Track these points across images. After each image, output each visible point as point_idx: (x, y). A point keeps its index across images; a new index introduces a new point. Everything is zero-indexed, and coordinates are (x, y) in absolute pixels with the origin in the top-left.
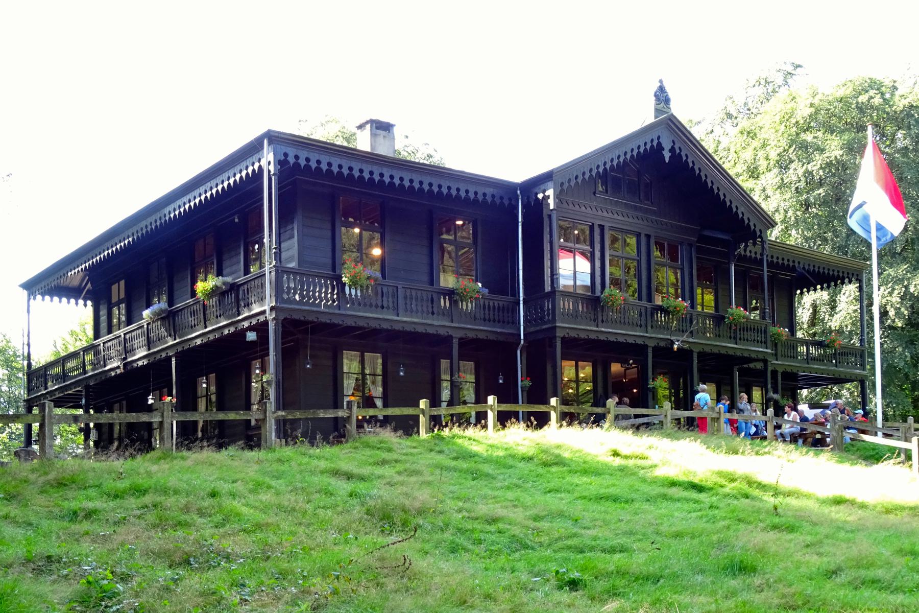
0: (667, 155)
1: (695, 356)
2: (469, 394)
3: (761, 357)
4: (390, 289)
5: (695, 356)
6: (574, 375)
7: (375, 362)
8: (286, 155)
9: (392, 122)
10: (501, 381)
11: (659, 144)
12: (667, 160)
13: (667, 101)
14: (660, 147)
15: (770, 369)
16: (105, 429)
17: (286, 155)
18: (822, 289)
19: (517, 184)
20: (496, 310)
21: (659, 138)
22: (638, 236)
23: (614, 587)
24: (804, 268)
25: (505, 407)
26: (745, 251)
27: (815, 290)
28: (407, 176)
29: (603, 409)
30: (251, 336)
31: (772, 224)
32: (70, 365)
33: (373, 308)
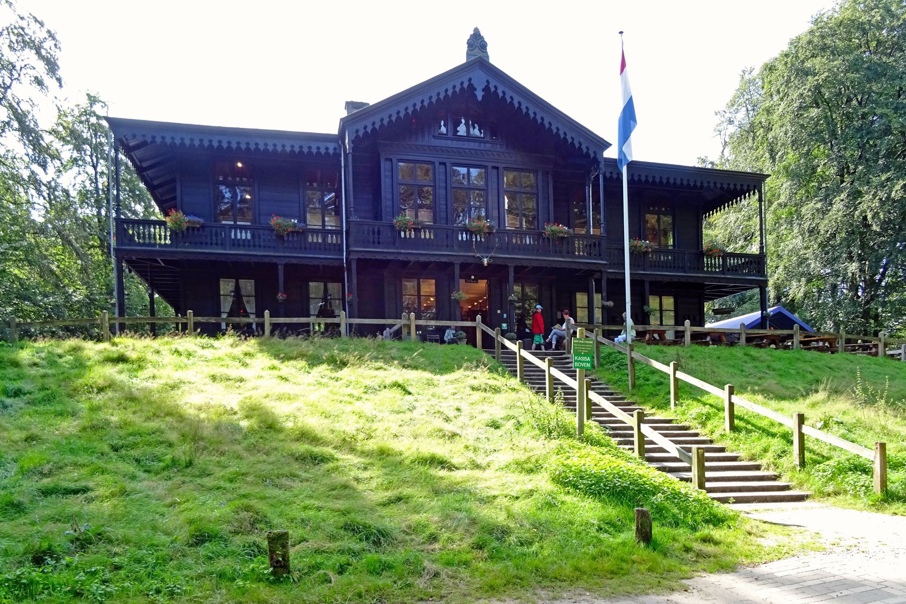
0: (480, 95)
2: (251, 308)
9: (344, 104)
13: (483, 46)
14: (472, 88)
20: (163, 237)
21: (470, 80)
24: (722, 188)
25: (641, 328)
29: (600, 321)
31: (606, 145)
33: (252, 248)
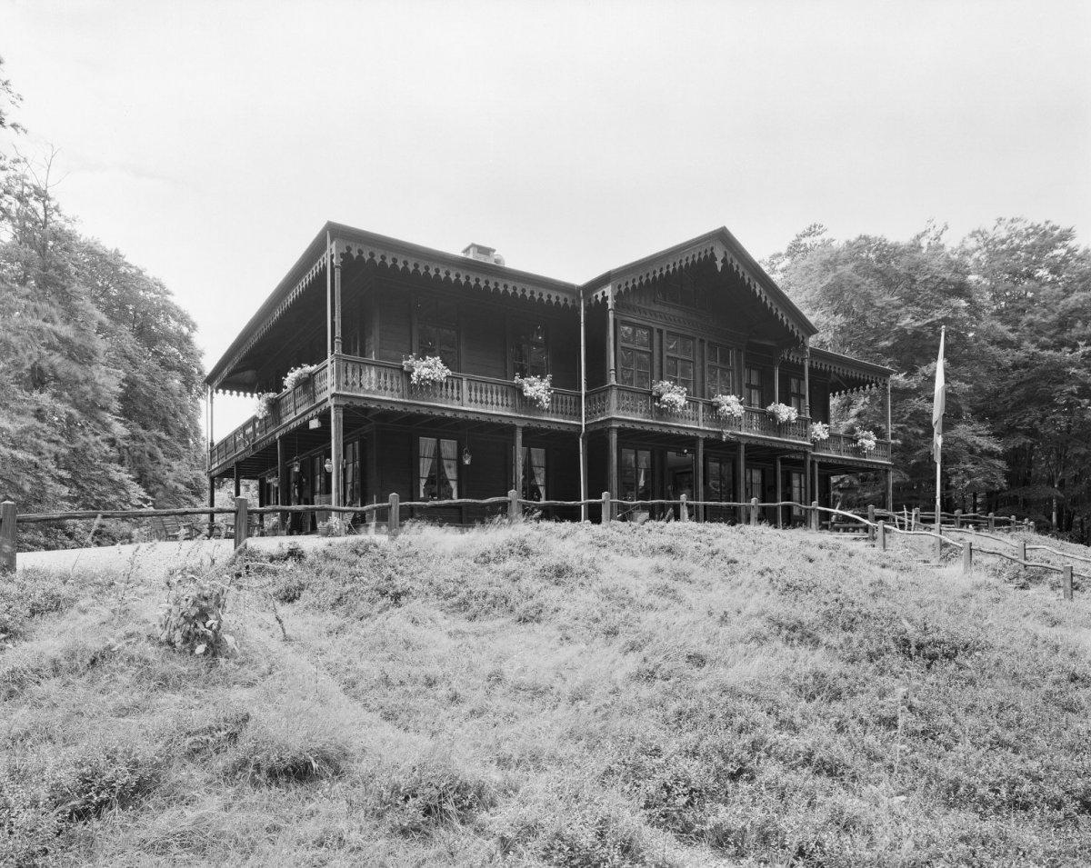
0: (719, 265)
1: (743, 448)
3: (801, 449)
4: (573, 399)
5: (743, 448)
6: (215, 494)
7: (449, 447)
8: (349, 249)
10: (467, 462)
11: (712, 254)
12: (720, 269)
14: (713, 258)
15: (809, 458)
17: (349, 249)
18: (840, 394)
21: (712, 249)
23: (915, 439)
26: (788, 356)
30: (314, 424)
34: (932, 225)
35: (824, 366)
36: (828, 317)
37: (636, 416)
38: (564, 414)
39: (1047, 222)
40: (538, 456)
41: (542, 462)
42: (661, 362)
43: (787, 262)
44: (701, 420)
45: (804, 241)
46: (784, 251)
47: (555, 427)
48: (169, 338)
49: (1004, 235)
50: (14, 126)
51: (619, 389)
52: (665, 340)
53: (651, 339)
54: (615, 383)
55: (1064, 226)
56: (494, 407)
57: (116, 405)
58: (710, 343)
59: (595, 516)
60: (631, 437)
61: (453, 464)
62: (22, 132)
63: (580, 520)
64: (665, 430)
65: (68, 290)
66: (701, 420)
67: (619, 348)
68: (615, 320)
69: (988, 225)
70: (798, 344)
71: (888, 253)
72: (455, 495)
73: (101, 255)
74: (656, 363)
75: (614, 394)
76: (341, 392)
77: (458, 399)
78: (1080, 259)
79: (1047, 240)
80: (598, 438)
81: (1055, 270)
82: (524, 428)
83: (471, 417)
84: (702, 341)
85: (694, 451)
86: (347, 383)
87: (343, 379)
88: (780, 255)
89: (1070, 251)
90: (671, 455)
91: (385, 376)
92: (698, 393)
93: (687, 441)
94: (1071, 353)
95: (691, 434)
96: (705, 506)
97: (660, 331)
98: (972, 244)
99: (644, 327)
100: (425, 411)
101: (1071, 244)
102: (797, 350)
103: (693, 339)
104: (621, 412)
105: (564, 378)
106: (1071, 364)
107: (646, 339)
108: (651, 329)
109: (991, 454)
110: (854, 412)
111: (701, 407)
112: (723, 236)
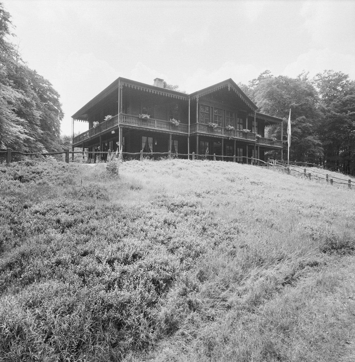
0: (229, 89)
5: (235, 142)
7: (150, 140)
10: (156, 144)
16: (105, 155)
17: (125, 84)
18: (270, 126)
19: (189, 95)
22: (209, 107)
27: (268, 126)
28: (169, 94)
30: (113, 132)
32: (81, 137)
34: (304, 72)
35: (259, 117)
36: (269, 101)
37: (204, 132)
38: (184, 131)
39: (340, 72)
40: (176, 143)
41: (152, 148)
42: (212, 116)
43: (258, 82)
44: (223, 133)
45: (263, 75)
46: (257, 79)
47: (181, 135)
48: (50, 99)
49: (327, 76)
50: (13, 34)
51: (199, 124)
52: (213, 109)
53: (209, 110)
54: (198, 123)
55: (346, 74)
56: (165, 129)
57: (39, 123)
58: (227, 111)
59: (191, 158)
60: (203, 138)
61: (151, 144)
62: (15, 36)
63: (187, 159)
64: (212, 136)
65: (24, 85)
66: (223, 133)
67: (200, 112)
68: (199, 104)
69: (322, 72)
70: (253, 112)
71: (288, 81)
72: (152, 152)
73: (30, 72)
74: (211, 115)
75: (198, 125)
76: (122, 124)
77: (154, 126)
78: (350, 84)
79: (341, 78)
80: (193, 138)
81: (343, 87)
82: (172, 135)
83: (157, 131)
84: (224, 110)
85: (221, 142)
86: (123, 121)
87: (122, 120)
88: (255, 80)
89: (347, 81)
90: (215, 143)
91: (132, 119)
92: (223, 125)
93: (219, 139)
94: (346, 114)
95: (220, 137)
96: (224, 157)
97: (212, 108)
98: (317, 78)
99: (207, 106)
100: (145, 129)
101: (348, 79)
102: (252, 113)
103: (222, 110)
104: (201, 131)
105: (184, 120)
106: (345, 117)
107: (208, 110)
108: (209, 107)
109: (318, 145)
110: (276, 131)
111: (223, 130)
112: (230, 81)
